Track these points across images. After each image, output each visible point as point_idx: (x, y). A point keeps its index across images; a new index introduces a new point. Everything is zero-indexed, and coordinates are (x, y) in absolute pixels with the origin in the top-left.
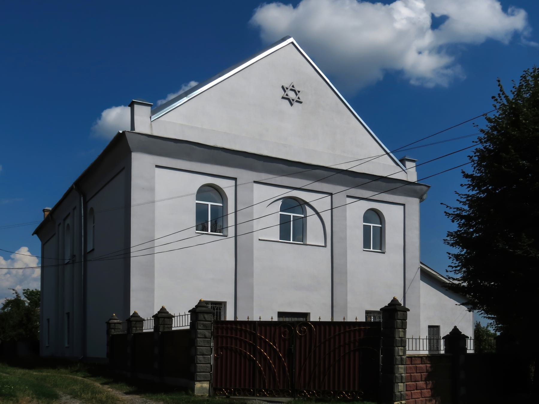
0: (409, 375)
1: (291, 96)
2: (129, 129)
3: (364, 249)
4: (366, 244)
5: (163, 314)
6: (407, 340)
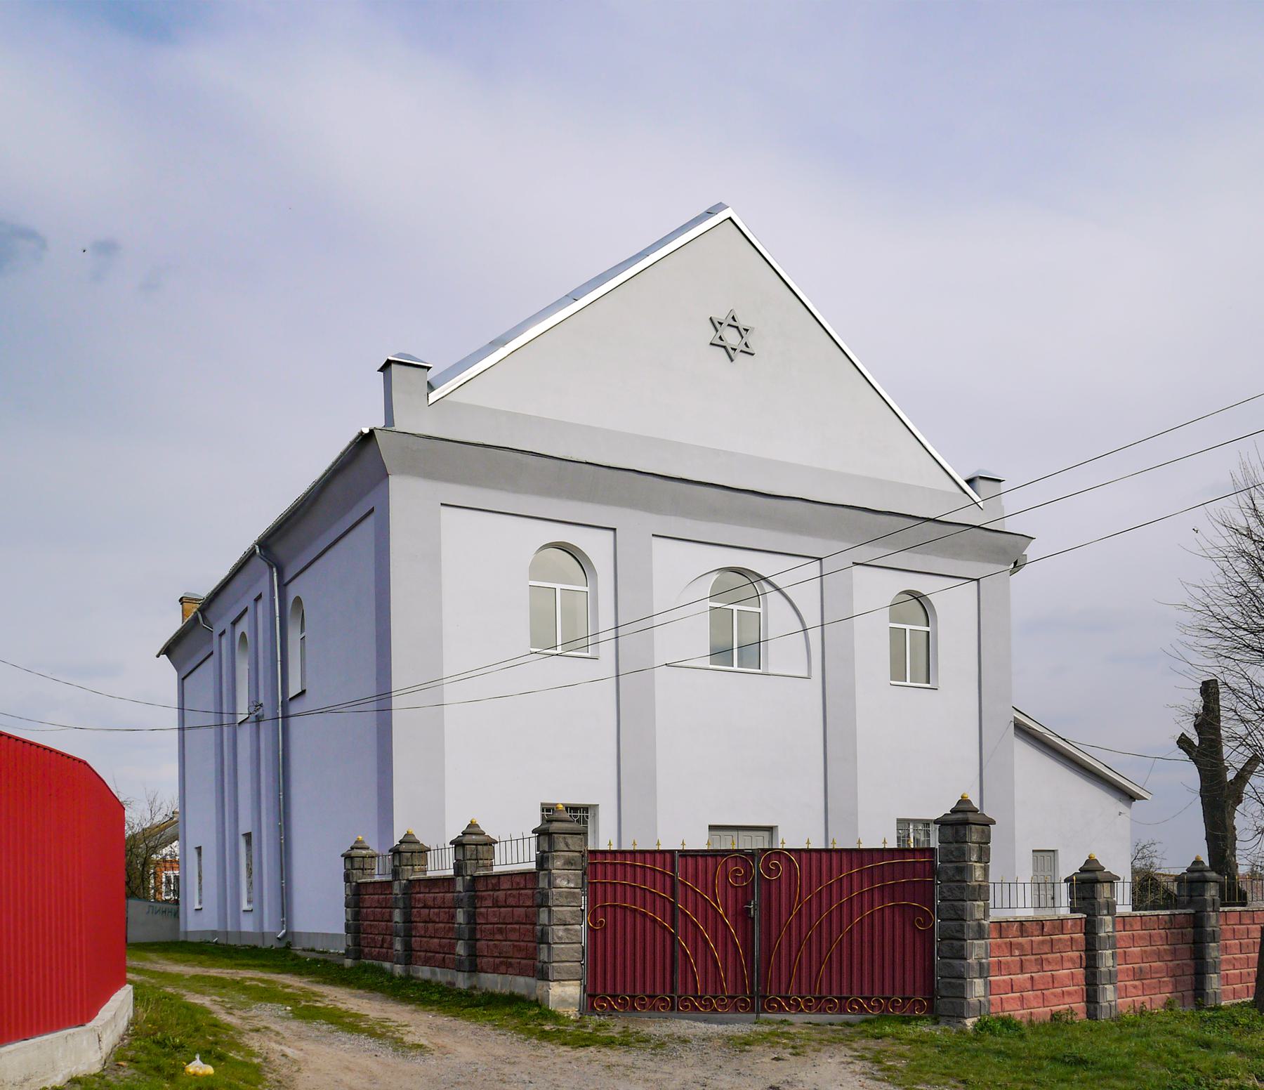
0: (995, 962)
1: (729, 342)
2: (379, 423)
3: (893, 682)
4: (898, 672)
5: (474, 837)
6: (991, 885)
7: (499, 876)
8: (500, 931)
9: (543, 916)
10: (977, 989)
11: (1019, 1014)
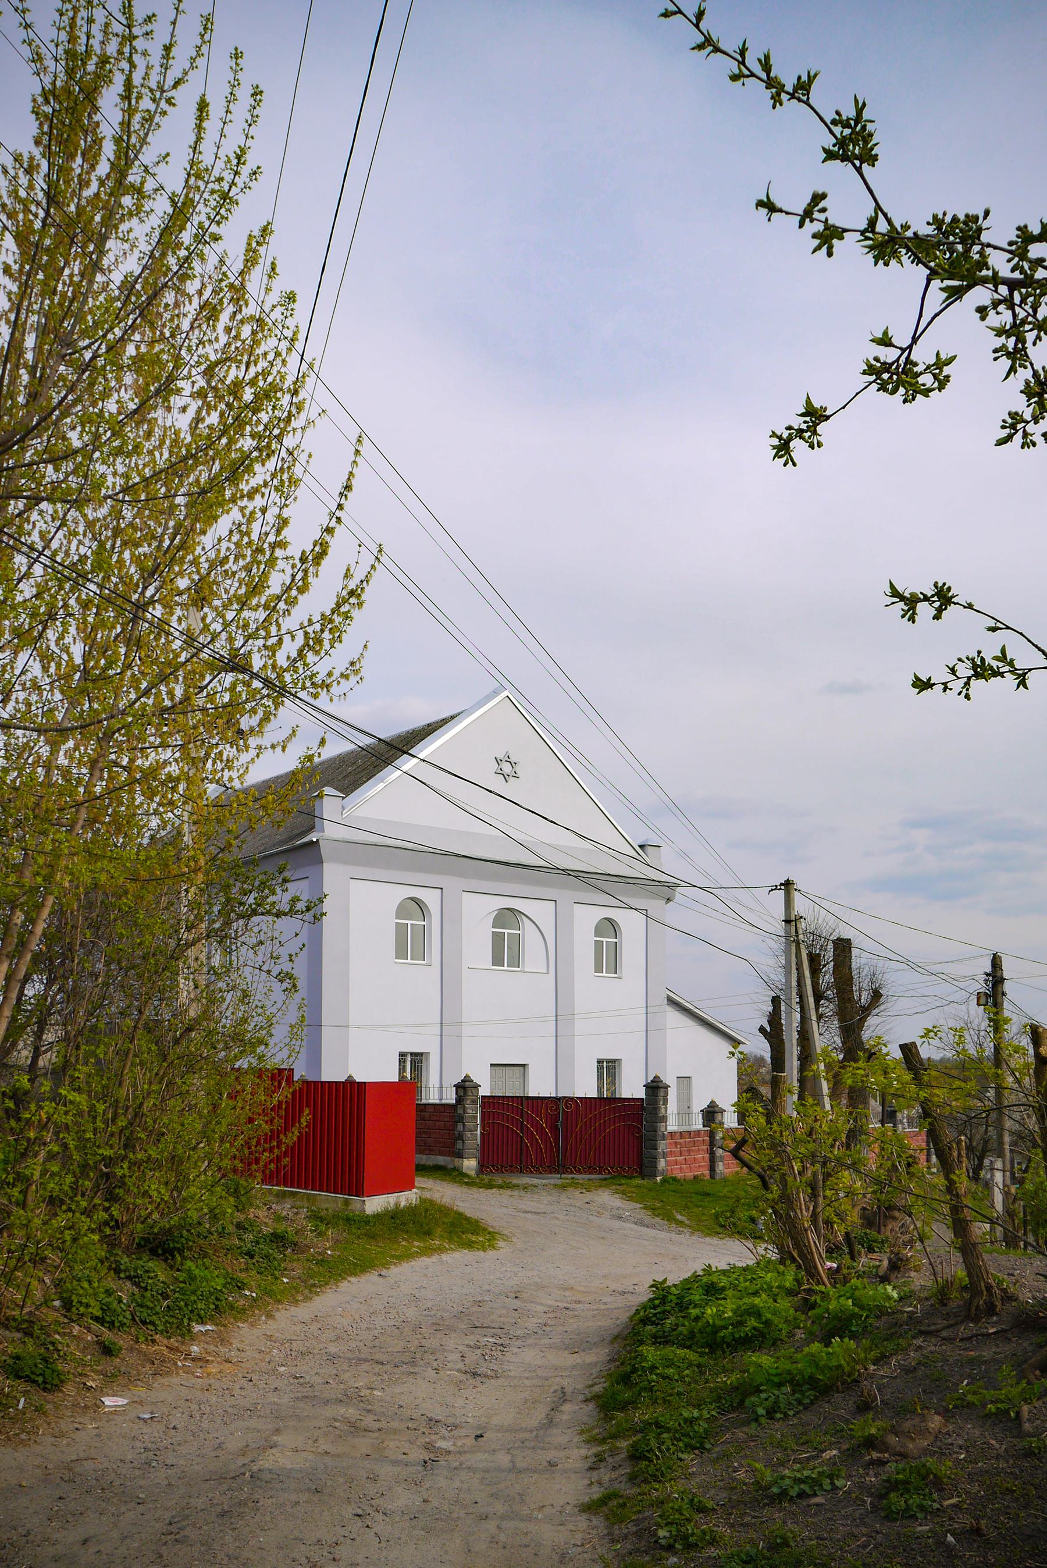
4: (598, 968)
7: (425, 1105)
8: (426, 1133)
9: (460, 1127)
10: (662, 1164)
11: (679, 1175)
